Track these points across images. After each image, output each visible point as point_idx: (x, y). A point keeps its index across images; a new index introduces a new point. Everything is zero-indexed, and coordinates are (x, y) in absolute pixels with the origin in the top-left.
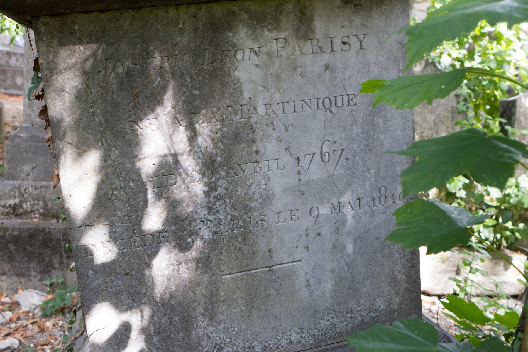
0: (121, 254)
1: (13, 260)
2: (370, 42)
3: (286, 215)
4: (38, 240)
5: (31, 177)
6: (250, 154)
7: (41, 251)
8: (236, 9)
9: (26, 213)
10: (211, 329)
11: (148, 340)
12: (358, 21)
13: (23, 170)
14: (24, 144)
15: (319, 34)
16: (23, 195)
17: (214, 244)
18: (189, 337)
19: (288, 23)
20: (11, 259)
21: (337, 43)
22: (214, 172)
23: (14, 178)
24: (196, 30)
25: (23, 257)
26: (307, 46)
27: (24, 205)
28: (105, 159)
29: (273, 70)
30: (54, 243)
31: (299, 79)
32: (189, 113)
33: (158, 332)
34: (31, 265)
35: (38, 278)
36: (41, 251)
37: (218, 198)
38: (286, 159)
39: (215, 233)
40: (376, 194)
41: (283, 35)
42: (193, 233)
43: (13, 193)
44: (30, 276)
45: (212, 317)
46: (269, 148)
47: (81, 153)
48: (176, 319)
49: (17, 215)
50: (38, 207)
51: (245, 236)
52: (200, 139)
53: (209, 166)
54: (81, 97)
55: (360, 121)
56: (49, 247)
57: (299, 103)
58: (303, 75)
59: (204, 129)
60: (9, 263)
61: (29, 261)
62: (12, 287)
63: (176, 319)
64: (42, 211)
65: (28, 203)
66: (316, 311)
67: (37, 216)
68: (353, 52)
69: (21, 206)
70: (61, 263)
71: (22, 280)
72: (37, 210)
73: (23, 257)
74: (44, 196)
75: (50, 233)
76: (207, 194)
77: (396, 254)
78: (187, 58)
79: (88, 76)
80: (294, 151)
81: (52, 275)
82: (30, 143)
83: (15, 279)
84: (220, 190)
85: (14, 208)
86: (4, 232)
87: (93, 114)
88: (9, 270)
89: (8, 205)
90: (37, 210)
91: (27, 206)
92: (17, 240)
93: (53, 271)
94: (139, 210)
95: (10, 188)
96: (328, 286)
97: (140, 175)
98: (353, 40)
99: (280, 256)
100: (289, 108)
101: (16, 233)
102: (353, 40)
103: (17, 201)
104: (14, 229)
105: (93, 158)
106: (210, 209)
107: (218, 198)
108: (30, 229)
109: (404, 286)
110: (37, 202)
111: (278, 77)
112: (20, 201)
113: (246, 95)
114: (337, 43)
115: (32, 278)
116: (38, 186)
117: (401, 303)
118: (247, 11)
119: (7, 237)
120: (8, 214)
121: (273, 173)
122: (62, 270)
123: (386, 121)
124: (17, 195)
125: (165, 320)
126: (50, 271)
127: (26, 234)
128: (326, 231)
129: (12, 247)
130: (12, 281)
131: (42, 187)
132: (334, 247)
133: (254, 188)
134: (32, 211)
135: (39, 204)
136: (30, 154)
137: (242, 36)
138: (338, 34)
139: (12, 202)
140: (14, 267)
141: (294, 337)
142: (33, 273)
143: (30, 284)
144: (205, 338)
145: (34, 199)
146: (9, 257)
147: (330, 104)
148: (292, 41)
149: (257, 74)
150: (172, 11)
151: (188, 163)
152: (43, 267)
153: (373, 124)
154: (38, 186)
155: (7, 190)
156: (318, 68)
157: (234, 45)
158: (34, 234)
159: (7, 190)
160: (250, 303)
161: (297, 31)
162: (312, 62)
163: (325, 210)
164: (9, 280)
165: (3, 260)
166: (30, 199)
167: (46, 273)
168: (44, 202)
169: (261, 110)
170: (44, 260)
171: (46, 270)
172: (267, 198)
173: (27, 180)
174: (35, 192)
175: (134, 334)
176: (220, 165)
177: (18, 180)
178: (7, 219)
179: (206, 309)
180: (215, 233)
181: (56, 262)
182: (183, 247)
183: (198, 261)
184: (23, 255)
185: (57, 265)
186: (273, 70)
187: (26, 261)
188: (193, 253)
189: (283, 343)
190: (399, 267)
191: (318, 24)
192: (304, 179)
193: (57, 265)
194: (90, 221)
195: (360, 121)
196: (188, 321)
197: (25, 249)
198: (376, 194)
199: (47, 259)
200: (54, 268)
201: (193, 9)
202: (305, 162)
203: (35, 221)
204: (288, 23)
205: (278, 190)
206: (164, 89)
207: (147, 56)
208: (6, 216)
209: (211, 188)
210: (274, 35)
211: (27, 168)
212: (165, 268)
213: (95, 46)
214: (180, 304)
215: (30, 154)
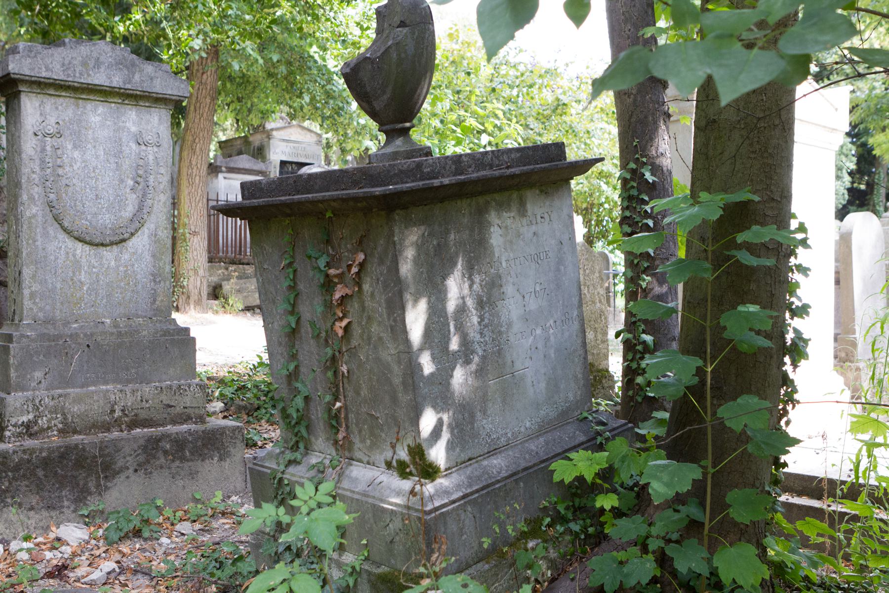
0: (438, 369)
1: (42, 489)
2: (554, 216)
3: (519, 335)
4: (71, 460)
5: (43, 385)
6: (500, 294)
7: (74, 473)
8: (489, 199)
9: (42, 430)
10: (485, 421)
11: (452, 433)
12: (548, 203)
13: (33, 377)
14: (34, 345)
15: (529, 213)
16: (38, 408)
17: (484, 358)
18: (473, 428)
19: (514, 208)
20: (40, 488)
21: (539, 219)
22: (482, 308)
23: (23, 389)
24: (471, 214)
25: (53, 484)
26: (524, 221)
27: (40, 422)
28: (429, 303)
29: (508, 238)
30: (88, 461)
31: (521, 243)
32: (470, 271)
33: (457, 426)
34: (63, 493)
35: (72, 509)
36: (74, 473)
37: (486, 326)
38: (518, 296)
39: (485, 351)
40: (563, 318)
41: (512, 214)
42: (473, 352)
43: (26, 407)
44: (63, 507)
45: (484, 412)
46: (509, 290)
47: (416, 301)
48: (466, 415)
49: (31, 436)
50: (56, 422)
51: (499, 352)
52: (475, 286)
53: (481, 304)
54: (416, 261)
55: (552, 269)
56: (84, 467)
57: (522, 258)
58: (523, 240)
59: (477, 279)
60: (38, 493)
61: (60, 489)
62: (41, 524)
63: (466, 415)
64: (60, 426)
65: (45, 418)
66: (538, 404)
67: (55, 433)
68: (546, 223)
69: (36, 423)
70: (98, 486)
71: (53, 513)
72: (55, 425)
73: (53, 484)
74: (63, 408)
75: (84, 449)
76: (479, 323)
77: (576, 359)
78: (467, 232)
79: (419, 247)
80: (521, 291)
81: (88, 502)
82: (39, 343)
83: (45, 513)
84: (486, 321)
85: (28, 426)
86: (30, 454)
87: (422, 273)
88: (38, 503)
89: (20, 423)
90: (55, 425)
91: (43, 422)
92: (46, 463)
93: (89, 498)
94: (447, 340)
95: (22, 401)
96: (543, 385)
97: (446, 313)
98: (546, 216)
99: (518, 365)
100: (517, 262)
101: (44, 454)
102: (546, 216)
103: (31, 416)
104: (41, 450)
105: (423, 305)
106: (481, 334)
107: (486, 326)
108: (60, 447)
109: (582, 382)
110: (54, 416)
111: (511, 242)
112: (35, 417)
113: (497, 255)
114: (539, 219)
115: (65, 510)
116: (56, 396)
117: (581, 395)
118: (495, 200)
119: (34, 460)
120: (20, 435)
121: (512, 308)
122: (100, 494)
123: (565, 267)
124: (30, 409)
125: (460, 416)
126: (85, 498)
127: (56, 454)
128: (540, 346)
129: (40, 473)
130: (40, 517)
131: (60, 396)
132: (545, 356)
133: (503, 318)
134: (49, 428)
135: (57, 418)
136: (41, 357)
137: (493, 217)
138: (539, 212)
139: (25, 419)
140: (43, 498)
141: (528, 424)
142: (66, 503)
143: (62, 517)
144: (481, 428)
145: (50, 412)
146: (37, 486)
147: (536, 258)
148: (517, 218)
149: (501, 240)
150: (459, 202)
151: (470, 303)
152: (76, 494)
153: (558, 270)
154: (56, 396)
155: (18, 405)
156: (530, 235)
157: (489, 223)
158: (65, 454)
159: (18, 405)
160: (504, 401)
161: (519, 211)
162: (527, 232)
163: (539, 331)
164: (37, 516)
165: (31, 491)
166: (47, 413)
167: (81, 501)
168: (64, 414)
169: (504, 264)
170: (78, 485)
171: (81, 498)
172: (510, 325)
173: (39, 389)
174: (52, 403)
175: (445, 428)
176: (486, 303)
177: (27, 391)
178: (19, 441)
179: (481, 407)
180: (485, 351)
181: (92, 485)
182: (468, 362)
183: (477, 371)
184: (53, 481)
185: (93, 489)
186: (508, 238)
187: (58, 489)
188: (473, 367)
189: (523, 429)
190: (578, 369)
191: (529, 206)
192: (527, 310)
193: (93, 489)
194: (421, 350)
195: (552, 269)
196: (472, 416)
197: (56, 473)
198: (563, 318)
199: (81, 483)
200: (90, 494)
201: (469, 201)
202: (527, 297)
203: (55, 440)
204: (514, 208)
205: (515, 318)
206: (457, 256)
207: (447, 232)
208: (18, 437)
209: (482, 318)
210: (508, 215)
211: (38, 375)
212: (459, 377)
213: (423, 228)
214: (468, 403)
215: (41, 357)
